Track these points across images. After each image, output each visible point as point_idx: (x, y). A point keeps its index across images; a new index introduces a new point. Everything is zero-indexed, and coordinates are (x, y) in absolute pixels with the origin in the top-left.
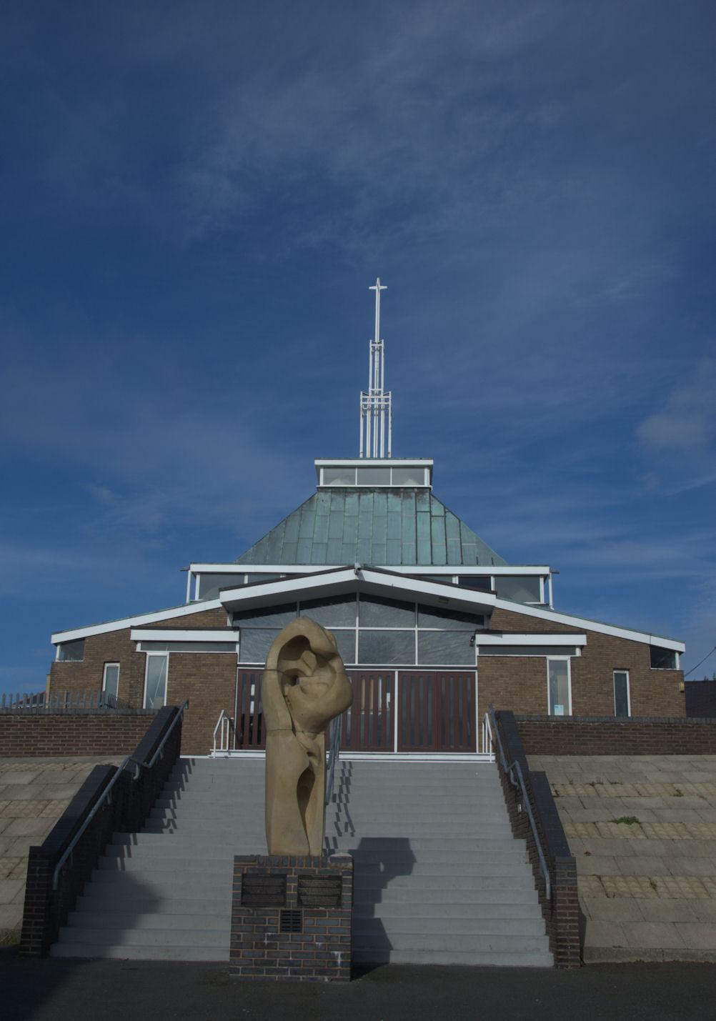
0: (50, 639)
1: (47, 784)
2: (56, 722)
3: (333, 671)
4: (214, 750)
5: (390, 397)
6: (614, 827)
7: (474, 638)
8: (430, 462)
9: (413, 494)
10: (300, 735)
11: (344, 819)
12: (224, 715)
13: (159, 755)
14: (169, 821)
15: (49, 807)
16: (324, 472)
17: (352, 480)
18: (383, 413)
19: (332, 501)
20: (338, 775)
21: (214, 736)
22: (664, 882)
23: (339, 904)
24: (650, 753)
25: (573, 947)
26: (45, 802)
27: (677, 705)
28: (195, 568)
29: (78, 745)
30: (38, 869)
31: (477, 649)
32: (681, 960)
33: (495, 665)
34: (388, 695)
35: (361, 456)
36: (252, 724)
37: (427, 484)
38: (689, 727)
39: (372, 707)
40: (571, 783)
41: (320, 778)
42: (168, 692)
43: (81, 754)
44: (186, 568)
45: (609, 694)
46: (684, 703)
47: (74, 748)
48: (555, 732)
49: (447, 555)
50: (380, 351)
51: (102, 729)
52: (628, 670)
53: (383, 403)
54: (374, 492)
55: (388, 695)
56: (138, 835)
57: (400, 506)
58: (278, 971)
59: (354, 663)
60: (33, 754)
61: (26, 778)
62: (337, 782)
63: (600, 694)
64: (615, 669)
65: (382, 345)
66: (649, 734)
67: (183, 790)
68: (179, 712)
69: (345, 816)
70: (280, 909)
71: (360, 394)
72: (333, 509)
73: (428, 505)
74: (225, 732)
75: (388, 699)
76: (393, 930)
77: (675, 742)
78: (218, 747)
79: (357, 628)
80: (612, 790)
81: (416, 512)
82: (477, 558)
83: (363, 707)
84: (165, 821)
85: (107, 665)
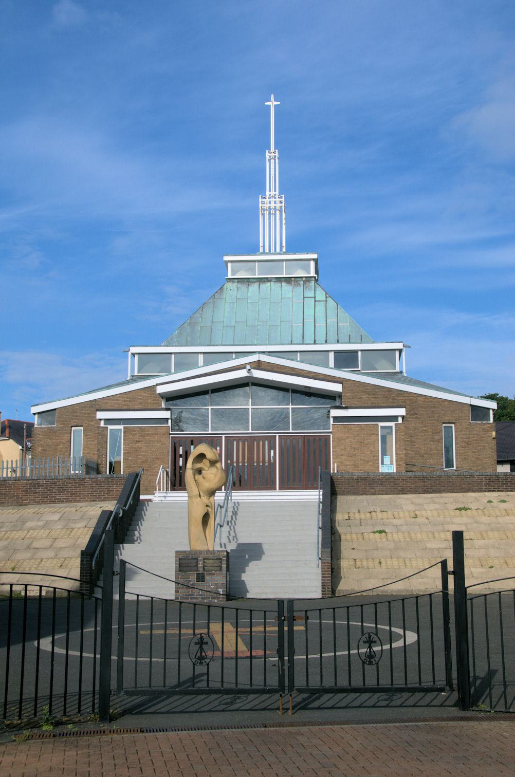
0: (30, 411)
1: (69, 520)
2: (67, 483)
3: (217, 467)
4: (157, 492)
5: (283, 200)
6: (372, 535)
7: (329, 411)
8: (315, 256)
9: (302, 283)
10: (202, 498)
11: (232, 534)
12: (162, 468)
13: (130, 503)
14: (137, 538)
15: (73, 532)
16: (232, 266)
17: (252, 270)
18: (278, 213)
19: (238, 290)
20: (230, 510)
21: (157, 484)
22: (386, 561)
23: (221, 570)
24: (411, 493)
25: (328, 588)
26: (71, 530)
27: (490, 448)
28: (134, 350)
29: (80, 496)
30: (85, 560)
31: (332, 420)
32: (380, 594)
33: (343, 430)
34: (272, 452)
35: (261, 250)
36: (181, 471)
37: (313, 274)
38: (434, 478)
39: (261, 460)
40: (359, 512)
41: (212, 516)
42: (124, 453)
43: (83, 501)
44: (127, 350)
45: (439, 441)
46: (496, 446)
47: (78, 498)
48: (357, 482)
49: (326, 334)
50: (275, 159)
51: (94, 487)
52: (454, 423)
53: (278, 205)
54: (271, 281)
55: (272, 452)
56: (125, 545)
57: (291, 294)
58: (195, 598)
59: (249, 430)
60: (54, 502)
61: (56, 517)
62: (230, 514)
63: (433, 441)
64: (444, 423)
65: (277, 154)
66: (411, 482)
67: (143, 520)
68: (139, 476)
69: (233, 533)
70: (195, 573)
71: (259, 198)
72: (238, 297)
73: (313, 292)
74: (163, 479)
75: (272, 454)
76: (249, 586)
77: (426, 486)
78: (159, 490)
79: (250, 407)
80: (380, 515)
81: (304, 298)
82: (350, 335)
83: (255, 461)
84: (135, 538)
85: (73, 428)
